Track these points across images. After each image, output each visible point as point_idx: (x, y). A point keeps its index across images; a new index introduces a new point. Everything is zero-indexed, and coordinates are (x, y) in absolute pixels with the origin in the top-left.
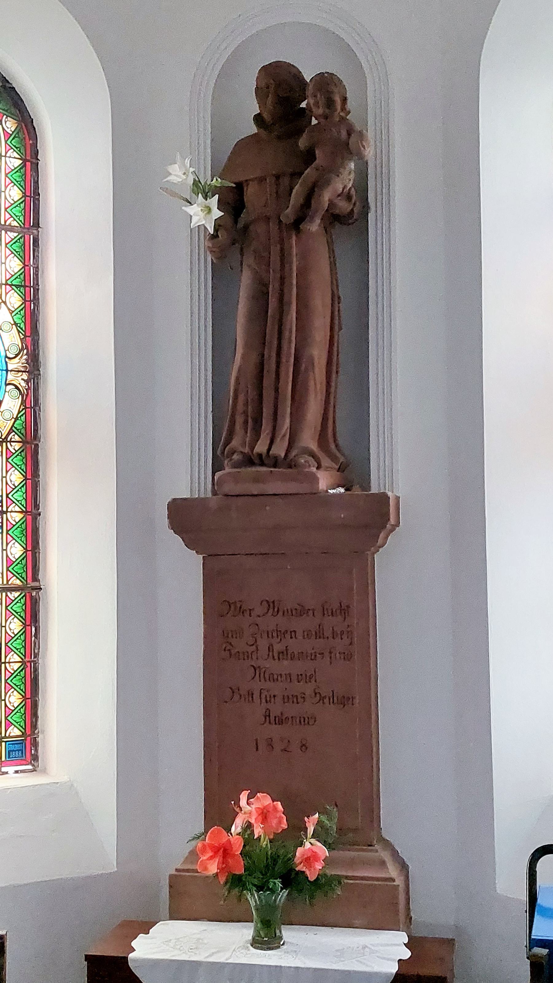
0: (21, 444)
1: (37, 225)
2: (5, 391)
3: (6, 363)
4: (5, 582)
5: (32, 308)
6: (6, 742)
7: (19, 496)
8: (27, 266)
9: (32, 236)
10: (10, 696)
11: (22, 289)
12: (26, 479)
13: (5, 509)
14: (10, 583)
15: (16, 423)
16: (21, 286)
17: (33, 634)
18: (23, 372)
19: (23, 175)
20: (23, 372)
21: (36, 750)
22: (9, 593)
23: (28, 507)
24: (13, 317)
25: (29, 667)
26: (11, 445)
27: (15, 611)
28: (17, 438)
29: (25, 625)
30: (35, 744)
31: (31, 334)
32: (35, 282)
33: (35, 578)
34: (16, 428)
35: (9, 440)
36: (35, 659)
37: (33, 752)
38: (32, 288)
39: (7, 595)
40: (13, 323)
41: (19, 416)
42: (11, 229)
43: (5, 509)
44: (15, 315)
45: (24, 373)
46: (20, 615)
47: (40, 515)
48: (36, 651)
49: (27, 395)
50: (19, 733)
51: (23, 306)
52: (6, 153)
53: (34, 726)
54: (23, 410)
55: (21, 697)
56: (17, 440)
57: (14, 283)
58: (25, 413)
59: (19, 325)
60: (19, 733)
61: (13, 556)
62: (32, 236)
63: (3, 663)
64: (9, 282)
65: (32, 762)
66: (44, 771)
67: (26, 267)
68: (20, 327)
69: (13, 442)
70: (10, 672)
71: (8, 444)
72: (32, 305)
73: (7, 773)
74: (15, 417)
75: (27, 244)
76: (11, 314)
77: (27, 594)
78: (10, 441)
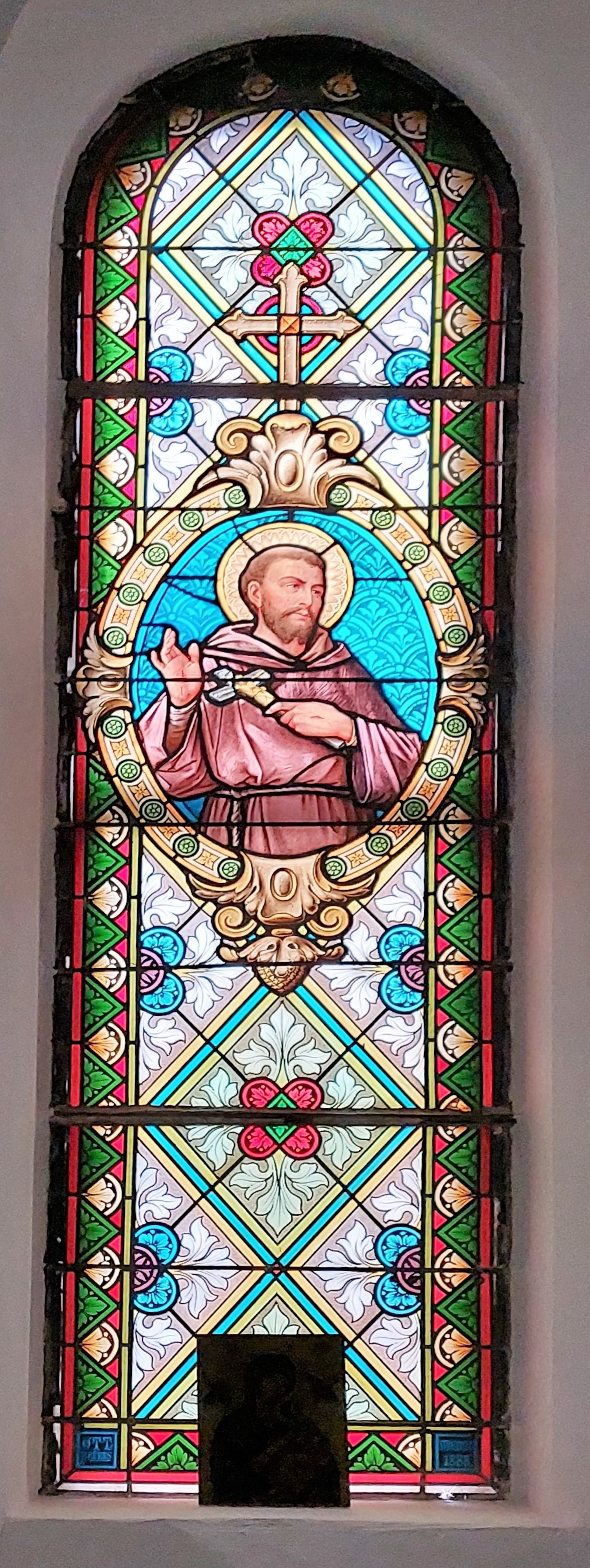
0: (469, 826)
1: (514, 377)
2: (436, 723)
4: (432, 1105)
5: (499, 549)
7: (463, 931)
8: (491, 464)
9: (502, 404)
11: (477, 514)
12: (479, 896)
13: (432, 957)
14: (442, 1107)
15: (459, 784)
16: (476, 507)
17: (496, 1213)
18: (475, 680)
20: (475, 680)
21: (505, 1456)
22: (441, 1130)
23: (484, 952)
24: (454, 572)
25: (487, 1282)
26: (447, 830)
27: (455, 1166)
29: (476, 1194)
30: (501, 1443)
31: (495, 603)
32: (508, 497)
33: (500, 1097)
34: (457, 794)
35: (442, 818)
36: (501, 1267)
37: (496, 1459)
38: (500, 511)
39: (436, 1132)
40: (454, 583)
42: (455, 392)
43: (432, 957)
47: (510, 968)
48: (504, 1250)
50: (467, 1418)
53: (500, 1406)
54: (474, 756)
55: (470, 1343)
58: (479, 763)
61: (122, 456)
62: (502, 404)
63: (428, 1270)
65: (496, 1480)
66: (524, 1502)
67: (489, 469)
68: (470, 590)
71: (441, 827)
72: (500, 543)
73: (437, 1496)
74: (456, 772)
76: (450, 566)
77: (483, 1131)
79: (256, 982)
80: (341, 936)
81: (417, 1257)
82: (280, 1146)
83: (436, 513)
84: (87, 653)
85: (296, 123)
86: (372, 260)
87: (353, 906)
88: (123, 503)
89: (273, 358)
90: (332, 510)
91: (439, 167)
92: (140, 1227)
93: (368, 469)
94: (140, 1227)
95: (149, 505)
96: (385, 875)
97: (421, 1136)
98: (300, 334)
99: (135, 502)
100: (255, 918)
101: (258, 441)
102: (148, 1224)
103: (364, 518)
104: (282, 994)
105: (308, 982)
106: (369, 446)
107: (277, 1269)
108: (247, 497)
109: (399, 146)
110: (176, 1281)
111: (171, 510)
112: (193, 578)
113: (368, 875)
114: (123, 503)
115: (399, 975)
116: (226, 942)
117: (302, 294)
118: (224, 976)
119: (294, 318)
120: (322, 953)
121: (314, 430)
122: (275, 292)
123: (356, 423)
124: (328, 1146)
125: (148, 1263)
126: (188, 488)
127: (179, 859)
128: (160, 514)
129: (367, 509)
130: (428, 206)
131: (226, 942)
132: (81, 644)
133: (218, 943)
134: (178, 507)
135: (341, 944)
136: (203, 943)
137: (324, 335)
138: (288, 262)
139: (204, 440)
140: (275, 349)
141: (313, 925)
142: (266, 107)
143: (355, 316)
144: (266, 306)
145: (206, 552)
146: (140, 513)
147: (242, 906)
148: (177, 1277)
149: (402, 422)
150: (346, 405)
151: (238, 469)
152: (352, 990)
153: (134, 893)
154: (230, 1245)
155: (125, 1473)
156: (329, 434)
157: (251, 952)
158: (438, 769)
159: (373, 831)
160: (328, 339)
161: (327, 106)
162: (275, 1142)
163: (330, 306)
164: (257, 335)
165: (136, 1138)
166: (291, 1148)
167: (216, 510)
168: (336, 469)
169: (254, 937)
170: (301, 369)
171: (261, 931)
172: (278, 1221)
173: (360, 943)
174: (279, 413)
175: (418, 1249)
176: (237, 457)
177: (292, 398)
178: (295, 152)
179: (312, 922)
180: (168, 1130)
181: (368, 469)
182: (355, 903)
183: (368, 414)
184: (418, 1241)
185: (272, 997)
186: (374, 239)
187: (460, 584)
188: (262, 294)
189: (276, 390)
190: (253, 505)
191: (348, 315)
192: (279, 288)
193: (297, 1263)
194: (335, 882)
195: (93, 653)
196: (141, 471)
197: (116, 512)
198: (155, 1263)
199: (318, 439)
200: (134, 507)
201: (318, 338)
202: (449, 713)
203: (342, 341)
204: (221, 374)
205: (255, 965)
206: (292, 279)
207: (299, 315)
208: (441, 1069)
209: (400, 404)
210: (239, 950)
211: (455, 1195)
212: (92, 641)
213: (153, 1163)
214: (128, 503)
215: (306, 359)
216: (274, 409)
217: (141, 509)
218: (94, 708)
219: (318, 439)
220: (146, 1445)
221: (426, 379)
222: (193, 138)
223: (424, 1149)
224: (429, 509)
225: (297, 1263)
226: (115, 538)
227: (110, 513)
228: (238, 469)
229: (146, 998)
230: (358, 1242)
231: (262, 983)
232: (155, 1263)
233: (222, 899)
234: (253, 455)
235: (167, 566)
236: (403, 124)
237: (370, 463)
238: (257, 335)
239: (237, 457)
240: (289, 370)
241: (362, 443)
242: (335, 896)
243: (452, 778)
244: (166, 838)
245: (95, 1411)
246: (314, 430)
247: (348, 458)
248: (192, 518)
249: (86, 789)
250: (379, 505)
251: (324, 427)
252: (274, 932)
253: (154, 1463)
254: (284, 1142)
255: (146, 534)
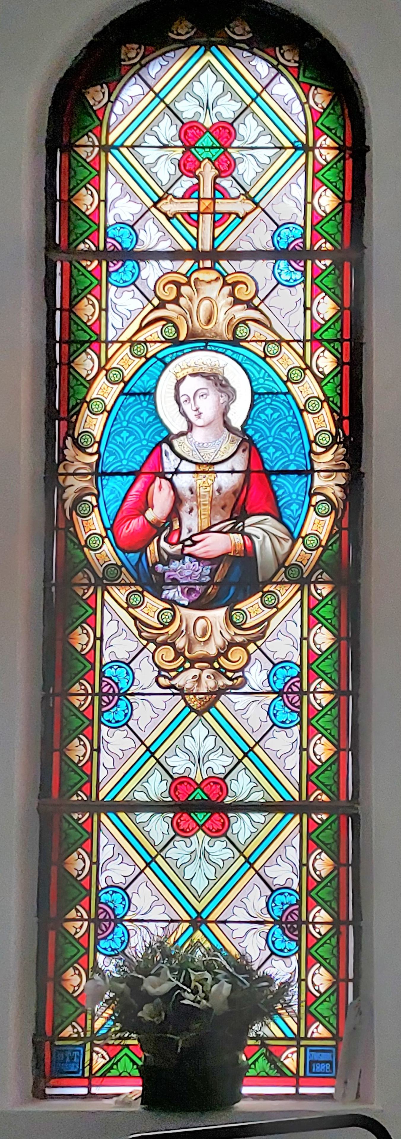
3: (311, 461)
6: (306, 1046)
10: (315, 744)
11: (337, 345)
19: (339, 117)
24: (321, 388)
27: (323, 671)
28: (324, 686)
35: (313, 579)
41: (330, 543)
44: (326, 384)
45: (339, 474)
46: (330, 678)
49: (343, 511)
50: (326, 1034)
51: (340, 207)
52: (315, 142)
54: (336, 533)
56: (331, 145)
57: (325, 336)
59: (331, 399)
60: (326, 1034)
64: (317, 336)
66: (366, 1102)
67: (342, 753)
68: (333, 402)
69: (321, 582)
70: (317, 599)
75: (343, 886)
76: (319, 384)
78: (317, 582)
79: (182, 704)
80: (242, 669)
81: (297, 912)
82: (200, 827)
83: (308, 344)
84: (66, 452)
85: (209, 57)
86: (263, 156)
87: (252, 647)
88: (91, 337)
89: (193, 231)
90: (236, 342)
91: (309, 86)
92: (102, 889)
93: (262, 313)
94: (102, 889)
95: (110, 339)
96: (274, 623)
97: (298, 821)
98: (214, 213)
99: (99, 335)
100: (183, 655)
101: (185, 290)
102: (108, 887)
103: (258, 348)
104: (200, 713)
105: (219, 705)
106: (262, 295)
107: (199, 922)
108: (177, 331)
109: (279, 72)
110: (128, 931)
111: (123, 343)
112: (139, 394)
113: (262, 622)
114: (91, 337)
115: (283, 699)
116: (163, 673)
117: (215, 183)
118: (158, 701)
119: (210, 201)
120: (230, 683)
121: (225, 284)
122: (195, 181)
123: (252, 277)
124: (235, 828)
125: (107, 917)
126: (135, 326)
127: (130, 610)
128: (117, 346)
129: (262, 341)
130: (301, 116)
131: (163, 673)
132: (61, 445)
133: (156, 674)
134: (130, 340)
135: (243, 676)
136: (145, 674)
137: (230, 214)
138: (204, 159)
139: (147, 289)
140: (195, 224)
141: (222, 660)
142: (187, 44)
143: (252, 200)
144: (189, 192)
145: (148, 375)
146: (103, 346)
147: (173, 645)
148: (129, 928)
149: (285, 277)
150: (245, 265)
151: (171, 311)
152: (248, 710)
153: (98, 635)
154: (169, 894)
155: (87, 1080)
156: (234, 285)
157: (178, 682)
158: (312, 542)
159: (265, 589)
160: (233, 216)
161: (231, 43)
162: (197, 824)
163: (234, 192)
164: (182, 214)
165: (99, 821)
166: (208, 829)
167: (155, 342)
168: (240, 312)
169: (182, 669)
170: (214, 239)
171: (187, 665)
172: (199, 884)
173: (256, 676)
174: (199, 269)
175: (297, 907)
176: (169, 302)
177: (208, 259)
178: (208, 76)
179: (222, 658)
180: (122, 815)
181: (262, 313)
182: (252, 645)
183: (261, 270)
184: (297, 900)
185: (193, 715)
186: (264, 141)
187: (327, 399)
188: (187, 183)
189: (196, 255)
190: (182, 338)
191: (247, 199)
192: (198, 178)
193: (212, 918)
194: (239, 628)
195: (70, 452)
196: (103, 313)
197: (87, 345)
198: (113, 917)
199: (227, 289)
200: (98, 341)
201: (227, 216)
202: (320, 498)
203: (243, 218)
204: (157, 244)
205: (181, 692)
206: (208, 172)
207: (214, 199)
208: (311, 770)
209: (283, 264)
210: (170, 679)
211: (322, 864)
212: (69, 442)
213: (112, 841)
214: (94, 338)
215: (218, 231)
216: (196, 267)
217: (103, 342)
218: (70, 494)
219: (227, 289)
220: (103, 1057)
221: (301, 245)
222: (138, 66)
223: (301, 832)
224: (304, 341)
225: (212, 918)
226: (87, 364)
227: (82, 346)
228: (171, 311)
229: (105, 714)
230: (256, 901)
231: (187, 705)
232: (113, 917)
233: (160, 639)
234: (182, 301)
235: (122, 385)
236: (282, 55)
237: (262, 307)
238: (182, 214)
239: (169, 302)
240: (205, 242)
241: (257, 291)
242: (238, 639)
243: (321, 549)
244: (121, 594)
245: (68, 1031)
246: (225, 284)
247: (249, 304)
248: (139, 349)
249: (65, 555)
250: (270, 338)
251: (230, 279)
252: (197, 665)
253: (108, 1071)
254: (204, 824)
255: (108, 360)
